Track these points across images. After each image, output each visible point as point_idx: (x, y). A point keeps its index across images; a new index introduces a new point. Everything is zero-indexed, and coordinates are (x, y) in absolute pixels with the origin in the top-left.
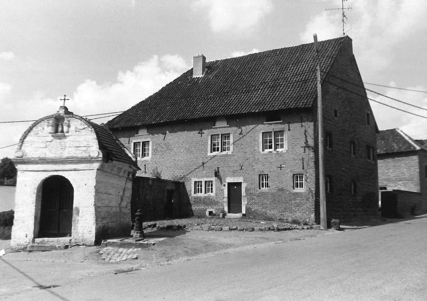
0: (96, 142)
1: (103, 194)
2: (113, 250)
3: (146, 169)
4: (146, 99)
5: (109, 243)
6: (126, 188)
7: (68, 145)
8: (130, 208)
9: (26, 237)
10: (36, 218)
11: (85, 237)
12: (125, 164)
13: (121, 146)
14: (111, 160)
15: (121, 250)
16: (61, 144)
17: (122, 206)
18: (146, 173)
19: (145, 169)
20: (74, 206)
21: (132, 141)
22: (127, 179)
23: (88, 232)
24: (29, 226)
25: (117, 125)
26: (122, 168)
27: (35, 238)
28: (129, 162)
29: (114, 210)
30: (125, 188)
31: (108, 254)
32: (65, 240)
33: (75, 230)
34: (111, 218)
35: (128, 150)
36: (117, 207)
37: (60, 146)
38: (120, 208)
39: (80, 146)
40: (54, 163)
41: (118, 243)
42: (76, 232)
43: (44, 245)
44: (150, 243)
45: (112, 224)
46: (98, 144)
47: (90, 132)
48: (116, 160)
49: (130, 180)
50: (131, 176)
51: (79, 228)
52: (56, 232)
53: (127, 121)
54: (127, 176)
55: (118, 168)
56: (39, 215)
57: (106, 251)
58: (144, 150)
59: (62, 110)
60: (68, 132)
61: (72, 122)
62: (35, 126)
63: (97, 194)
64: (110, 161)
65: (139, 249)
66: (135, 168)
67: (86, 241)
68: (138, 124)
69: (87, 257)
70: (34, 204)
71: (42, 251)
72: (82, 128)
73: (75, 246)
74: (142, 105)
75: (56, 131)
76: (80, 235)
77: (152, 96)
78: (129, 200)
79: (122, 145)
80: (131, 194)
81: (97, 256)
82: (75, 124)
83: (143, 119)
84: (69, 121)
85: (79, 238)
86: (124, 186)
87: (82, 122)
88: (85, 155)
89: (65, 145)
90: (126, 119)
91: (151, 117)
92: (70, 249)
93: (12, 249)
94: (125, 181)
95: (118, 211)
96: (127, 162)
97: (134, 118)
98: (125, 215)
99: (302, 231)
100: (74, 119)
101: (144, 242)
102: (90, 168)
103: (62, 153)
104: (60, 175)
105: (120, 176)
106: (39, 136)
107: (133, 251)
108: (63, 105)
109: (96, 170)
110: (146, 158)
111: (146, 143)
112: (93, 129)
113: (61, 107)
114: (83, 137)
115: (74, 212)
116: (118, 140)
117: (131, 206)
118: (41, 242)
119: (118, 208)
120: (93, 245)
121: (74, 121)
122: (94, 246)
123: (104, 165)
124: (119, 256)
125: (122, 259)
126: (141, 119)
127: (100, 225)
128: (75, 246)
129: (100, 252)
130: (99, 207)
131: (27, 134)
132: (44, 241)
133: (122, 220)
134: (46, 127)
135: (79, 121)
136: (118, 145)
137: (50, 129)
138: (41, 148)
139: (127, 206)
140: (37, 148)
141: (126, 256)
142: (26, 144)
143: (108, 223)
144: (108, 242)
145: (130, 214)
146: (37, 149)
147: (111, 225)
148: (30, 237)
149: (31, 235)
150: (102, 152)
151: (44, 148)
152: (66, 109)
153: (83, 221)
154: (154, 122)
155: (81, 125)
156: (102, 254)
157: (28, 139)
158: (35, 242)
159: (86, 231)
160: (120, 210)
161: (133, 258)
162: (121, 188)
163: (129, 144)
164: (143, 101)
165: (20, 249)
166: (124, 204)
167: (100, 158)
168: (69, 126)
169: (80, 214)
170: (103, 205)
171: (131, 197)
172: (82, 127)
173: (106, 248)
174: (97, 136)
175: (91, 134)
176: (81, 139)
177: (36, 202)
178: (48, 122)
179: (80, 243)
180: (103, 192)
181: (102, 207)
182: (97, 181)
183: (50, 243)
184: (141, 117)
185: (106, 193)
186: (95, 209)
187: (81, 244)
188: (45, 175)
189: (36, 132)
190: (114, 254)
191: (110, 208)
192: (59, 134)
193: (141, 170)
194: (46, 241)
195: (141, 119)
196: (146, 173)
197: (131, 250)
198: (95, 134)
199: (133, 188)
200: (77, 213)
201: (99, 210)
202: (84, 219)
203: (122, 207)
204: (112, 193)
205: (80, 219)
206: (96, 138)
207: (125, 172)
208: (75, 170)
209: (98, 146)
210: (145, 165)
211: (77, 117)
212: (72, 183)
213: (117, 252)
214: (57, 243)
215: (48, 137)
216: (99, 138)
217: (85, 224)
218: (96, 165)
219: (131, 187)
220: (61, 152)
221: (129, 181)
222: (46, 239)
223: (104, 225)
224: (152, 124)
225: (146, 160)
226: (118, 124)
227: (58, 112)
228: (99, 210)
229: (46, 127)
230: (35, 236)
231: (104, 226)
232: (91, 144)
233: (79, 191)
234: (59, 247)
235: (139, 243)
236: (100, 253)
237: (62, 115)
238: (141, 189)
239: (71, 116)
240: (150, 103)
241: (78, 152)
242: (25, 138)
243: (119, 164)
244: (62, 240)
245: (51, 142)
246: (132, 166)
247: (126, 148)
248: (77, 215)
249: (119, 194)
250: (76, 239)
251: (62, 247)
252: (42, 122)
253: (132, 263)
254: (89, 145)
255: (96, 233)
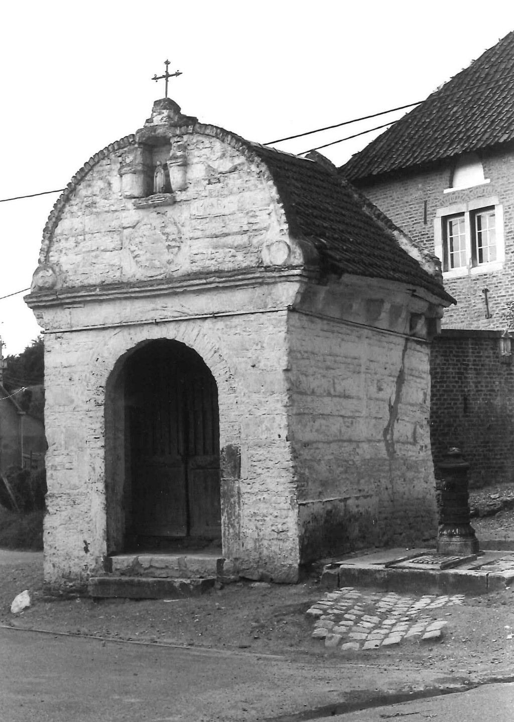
0: (279, 211)
1: (321, 396)
2: (358, 600)
3: (490, 305)
4: (475, 63)
5: (347, 572)
6: (406, 371)
7: (187, 232)
8: (428, 441)
9: (86, 550)
10: (109, 488)
11: (265, 552)
12: (390, 285)
13: (381, 223)
14: (335, 273)
15: (389, 600)
16: (167, 230)
17: (395, 437)
18: (489, 316)
19: (487, 304)
20: (223, 443)
21: (434, 214)
22: (407, 340)
23: (275, 535)
24: (92, 513)
25: (380, 163)
26: (382, 301)
27: (111, 553)
28: (404, 277)
29: (366, 451)
30: (402, 372)
31: (338, 618)
32: (199, 562)
33: (233, 526)
34: (358, 483)
35: (405, 236)
36: (379, 441)
37: (164, 238)
38: (390, 446)
39: (225, 231)
40: (148, 297)
41: (378, 576)
42: (237, 536)
43: (136, 579)
44: (498, 573)
45: (362, 501)
46: (284, 218)
47: (253, 179)
48: (355, 273)
49: (418, 343)
50: (421, 328)
51: (244, 521)
52: (182, 534)
53: (413, 145)
54: (408, 331)
55: (370, 301)
56: (121, 478)
57: (331, 607)
58: (476, 240)
59: (160, 114)
60: (184, 189)
61: (196, 153)
62: (82, 179)
63: (295, 396)
64: (334, 276)
65: (457, 599)
66: (434, 300)
67: (269, 567)
68: (451, 153)
69: (263, 626)
70: (101, 443)
71: (131, 599)
72: (227, 169)
73: (235, 582)
74: (462, 84)
75: (149, 190)
76: (250, 545)
77: (492, 49)
78: (423, 417)
79: (382, 220)
80: (429, 392)
81: (299, 625)
82: (206, 156)
83: (468, 130)
84: (184, 148)
85: (248, 555)
86: (399, 366)
87: (225, 145)
88: (243, 261)
89: (179, 232)
90: (411, 138)
91: (493, 122)
92: (220, 593)
93: (49, 589)
94: (401, 348)
95: (384, 453)
96: (397, 275)
97: (435, 131)
98: (409, 468)
99: (468, 694)
100: (201, 138)
101: (473, 573)
102: (266, 307)
103: (169, 262)
104: (170, 336)
105: (381, 332)
106: (98, 214)
107: (433, 606)
108: (163, 97)
109: (285, 312)
110: (482, 268)
111: (482, 214)
112: (264, 168)
113: (157, 103)
114: (231, 198)
115: (225, 466)
116: (370, 206)
117: (432, 435)
118: (134, 569)
119: (382, 445)
120: (295, 580)
121: (201, 146)
122: (297, 583)
123: (315, 294)
124: (378, 626)
125: (387, 642)
126: (460, 132)
127: (316, 506)
128: (235, 581)
129: (309, 611)
130: (306, 445)
131: (61, 211)
132: (137, 563)
133: (401, 487)
134: (115, 180)
135: (218, 145)
136: (368, 221)
137: (130, 184)
138: (105, 251)
139: (418, 435)
140: (94, 254)
141: (402, 627)
142: (63, 244)
143: (346, 499)
144: (345, 570)
145: (431, 464)
146: (96, 257)
147: (357, 506)
148: (97, 553)
149: (99, 547)
150: (302, 246)
151: (114, 249)
152: (170, 105)
153: (256, 494)
154: (506, 136)
155: (223, 155)
156: (317, 617)
157: (65, 225)
158: (114, 566)
159: (267, 530)
160: (391, 453)
161: (427, 635)
162: (387, 372)
163: (425, 223)
164: (465, 73)
165: (72, 592)
166: (403, 429)
167: (294, 268)
168: (185, 165)
169: (244, 474)
170: (321, 437)
171: (428, 403)
172: (227, 165)
173: (335, 595)
174: (280, 191)
175: (260, 186)
176: (229, 204)
177: (105, 435)
178: (120, 159)
179: (252, 574)
180: (319, 391)
181: (320, 445)
182: (291, 352)
183: (158, 572)
184: (459, 125)
185: (329, 394)
186: (294, 451)
187: (255, 577)
188: (119, 344)
189: (90, 200)
190: (359, 619)
191: (348, 448)
192: (157, 198)
193: (455, 303)
194: (146, 565)
195: (460, 132)
196: (489, 316)
197: (423, 602)
198: (271, 183)
199: (433, 373)
200: (235, 467)
201: (306, 454)
202: (257, 487)
203: (398, 442)
204: (353, 393)
205: (244, 488)
206: (277, 196)
207: (395, 312)
208: (215, 316)
209: (286, 226)
210: (486, 291)
211: (208, 131)
212: (208, 363)
213: (370, 610)
214: (177, 574)
215: (124, 214)
216: (286, 197)
217: (262, 505)
218: (288, 292)
219: (427, 367)
220: (171, 257)
221: (418, 347)
222: (145, 558)
223: (329, 507)
224: (497, 143)
225: (485, 271)
226: (384, 159)
227: (147, 121)
228: (306, 454)
229: (115, 180)
230: (113, 548)
231: (329, 513)
232: (263, 219)
233: (233, 389)
234: (183, 585)
235: (456, 575)
236: (310, 615)
237: (160, 131)
238: (471, 375)
239: (190, 128)
240: (487, 74)
241: (221, 254)
242: (56, 225)
243: (369, 286)
244: (191, 561)
245: (134, 227)
246: (421, 292)
247: (396, 228)
248: (233, 474)
249: (381, 395)
250: (236, 559)
251: (192, 587)
252: (104, 162)
253: (420, 658)
254: (255, 227)
255: (302, 538)
